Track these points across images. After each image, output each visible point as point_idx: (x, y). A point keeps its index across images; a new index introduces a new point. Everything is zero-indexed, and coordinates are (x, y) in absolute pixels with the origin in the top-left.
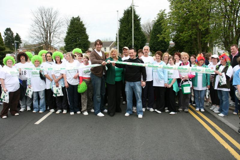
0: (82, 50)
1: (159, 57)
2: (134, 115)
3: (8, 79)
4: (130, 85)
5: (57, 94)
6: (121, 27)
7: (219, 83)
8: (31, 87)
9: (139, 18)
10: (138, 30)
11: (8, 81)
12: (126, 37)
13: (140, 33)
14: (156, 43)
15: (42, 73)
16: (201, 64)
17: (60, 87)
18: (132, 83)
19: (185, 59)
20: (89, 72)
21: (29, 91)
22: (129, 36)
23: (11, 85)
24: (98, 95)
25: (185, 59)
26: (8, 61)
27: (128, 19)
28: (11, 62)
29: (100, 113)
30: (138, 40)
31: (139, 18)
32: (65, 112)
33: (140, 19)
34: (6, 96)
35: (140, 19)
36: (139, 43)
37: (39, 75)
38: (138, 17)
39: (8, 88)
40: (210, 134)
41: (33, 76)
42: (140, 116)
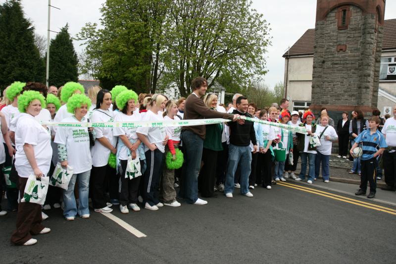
0: (84, 87)
1: (253, 109)
2: (241, 193)
3: (42, 145)
4: (240, 151)
5: (134, 173)
6: (33, 46)
7: (310, 145)
8: (68, 166)
9: (30, 27)
10: (31, 50)
11: (42, 150)
12: (4, 59)
13: (34, 55)
14: (55, 77)
15: (94, 133)
16: (286, 121)
17: (137, 160)
18: (244, 147)
19: (275, 115)
20: (178, 132)
21: (64, 175)
22: (10, 58)
23: (46, 160)
24: (197, 169)
25: (275, 115)
26: (34, 103)
27: (9, 24)
28: (53, 108)
29: (199, 199)
30: (30, 69)
31: (30, 27)
32: (136, 208)
33: (33, 28)
34: (42, 187)
35: (33, 28)
36: (31, 73)
37: (16, 142)
38: (30, 24)
39: (41, 167)
40: (344, 202)
41: (77, 139)
42: (230, 195)
